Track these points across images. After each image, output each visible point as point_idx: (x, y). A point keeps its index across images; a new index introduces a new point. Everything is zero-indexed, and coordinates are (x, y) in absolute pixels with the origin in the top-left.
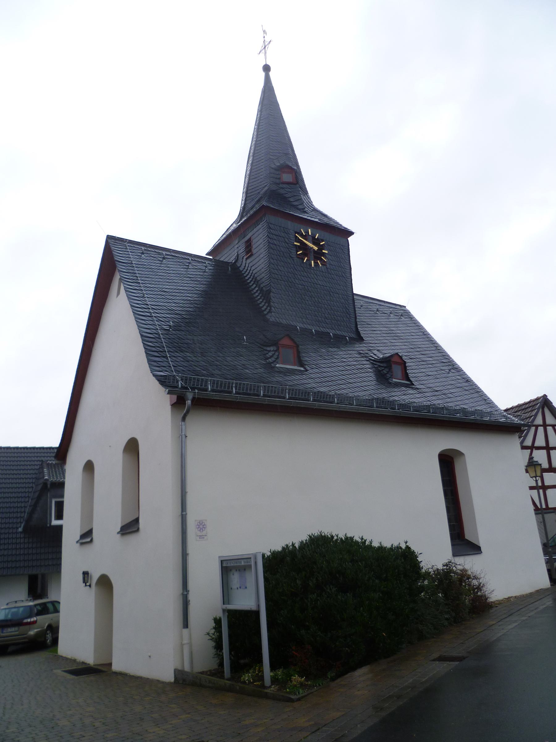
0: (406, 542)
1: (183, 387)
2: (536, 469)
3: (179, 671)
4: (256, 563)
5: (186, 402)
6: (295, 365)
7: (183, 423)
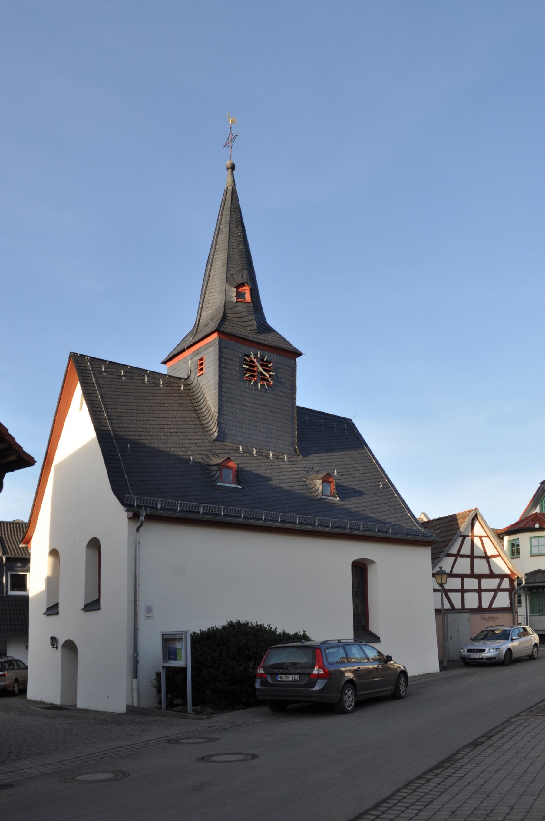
0: (305, 632)
1: (138, 506)
2: (443, 577)
3: (130, 706)
4: (186, 637)
5: (140, 518)
6: (233, 483)
7: (138, 533)
